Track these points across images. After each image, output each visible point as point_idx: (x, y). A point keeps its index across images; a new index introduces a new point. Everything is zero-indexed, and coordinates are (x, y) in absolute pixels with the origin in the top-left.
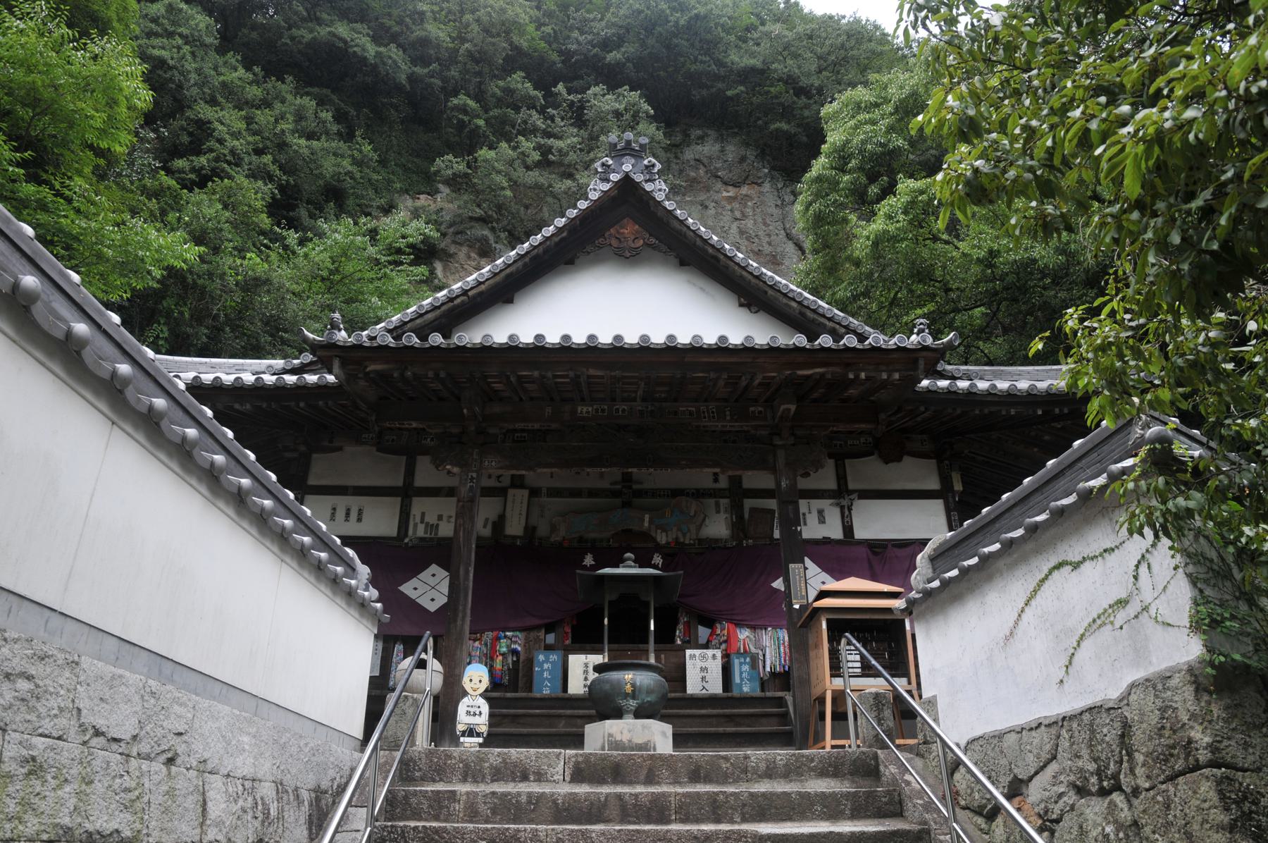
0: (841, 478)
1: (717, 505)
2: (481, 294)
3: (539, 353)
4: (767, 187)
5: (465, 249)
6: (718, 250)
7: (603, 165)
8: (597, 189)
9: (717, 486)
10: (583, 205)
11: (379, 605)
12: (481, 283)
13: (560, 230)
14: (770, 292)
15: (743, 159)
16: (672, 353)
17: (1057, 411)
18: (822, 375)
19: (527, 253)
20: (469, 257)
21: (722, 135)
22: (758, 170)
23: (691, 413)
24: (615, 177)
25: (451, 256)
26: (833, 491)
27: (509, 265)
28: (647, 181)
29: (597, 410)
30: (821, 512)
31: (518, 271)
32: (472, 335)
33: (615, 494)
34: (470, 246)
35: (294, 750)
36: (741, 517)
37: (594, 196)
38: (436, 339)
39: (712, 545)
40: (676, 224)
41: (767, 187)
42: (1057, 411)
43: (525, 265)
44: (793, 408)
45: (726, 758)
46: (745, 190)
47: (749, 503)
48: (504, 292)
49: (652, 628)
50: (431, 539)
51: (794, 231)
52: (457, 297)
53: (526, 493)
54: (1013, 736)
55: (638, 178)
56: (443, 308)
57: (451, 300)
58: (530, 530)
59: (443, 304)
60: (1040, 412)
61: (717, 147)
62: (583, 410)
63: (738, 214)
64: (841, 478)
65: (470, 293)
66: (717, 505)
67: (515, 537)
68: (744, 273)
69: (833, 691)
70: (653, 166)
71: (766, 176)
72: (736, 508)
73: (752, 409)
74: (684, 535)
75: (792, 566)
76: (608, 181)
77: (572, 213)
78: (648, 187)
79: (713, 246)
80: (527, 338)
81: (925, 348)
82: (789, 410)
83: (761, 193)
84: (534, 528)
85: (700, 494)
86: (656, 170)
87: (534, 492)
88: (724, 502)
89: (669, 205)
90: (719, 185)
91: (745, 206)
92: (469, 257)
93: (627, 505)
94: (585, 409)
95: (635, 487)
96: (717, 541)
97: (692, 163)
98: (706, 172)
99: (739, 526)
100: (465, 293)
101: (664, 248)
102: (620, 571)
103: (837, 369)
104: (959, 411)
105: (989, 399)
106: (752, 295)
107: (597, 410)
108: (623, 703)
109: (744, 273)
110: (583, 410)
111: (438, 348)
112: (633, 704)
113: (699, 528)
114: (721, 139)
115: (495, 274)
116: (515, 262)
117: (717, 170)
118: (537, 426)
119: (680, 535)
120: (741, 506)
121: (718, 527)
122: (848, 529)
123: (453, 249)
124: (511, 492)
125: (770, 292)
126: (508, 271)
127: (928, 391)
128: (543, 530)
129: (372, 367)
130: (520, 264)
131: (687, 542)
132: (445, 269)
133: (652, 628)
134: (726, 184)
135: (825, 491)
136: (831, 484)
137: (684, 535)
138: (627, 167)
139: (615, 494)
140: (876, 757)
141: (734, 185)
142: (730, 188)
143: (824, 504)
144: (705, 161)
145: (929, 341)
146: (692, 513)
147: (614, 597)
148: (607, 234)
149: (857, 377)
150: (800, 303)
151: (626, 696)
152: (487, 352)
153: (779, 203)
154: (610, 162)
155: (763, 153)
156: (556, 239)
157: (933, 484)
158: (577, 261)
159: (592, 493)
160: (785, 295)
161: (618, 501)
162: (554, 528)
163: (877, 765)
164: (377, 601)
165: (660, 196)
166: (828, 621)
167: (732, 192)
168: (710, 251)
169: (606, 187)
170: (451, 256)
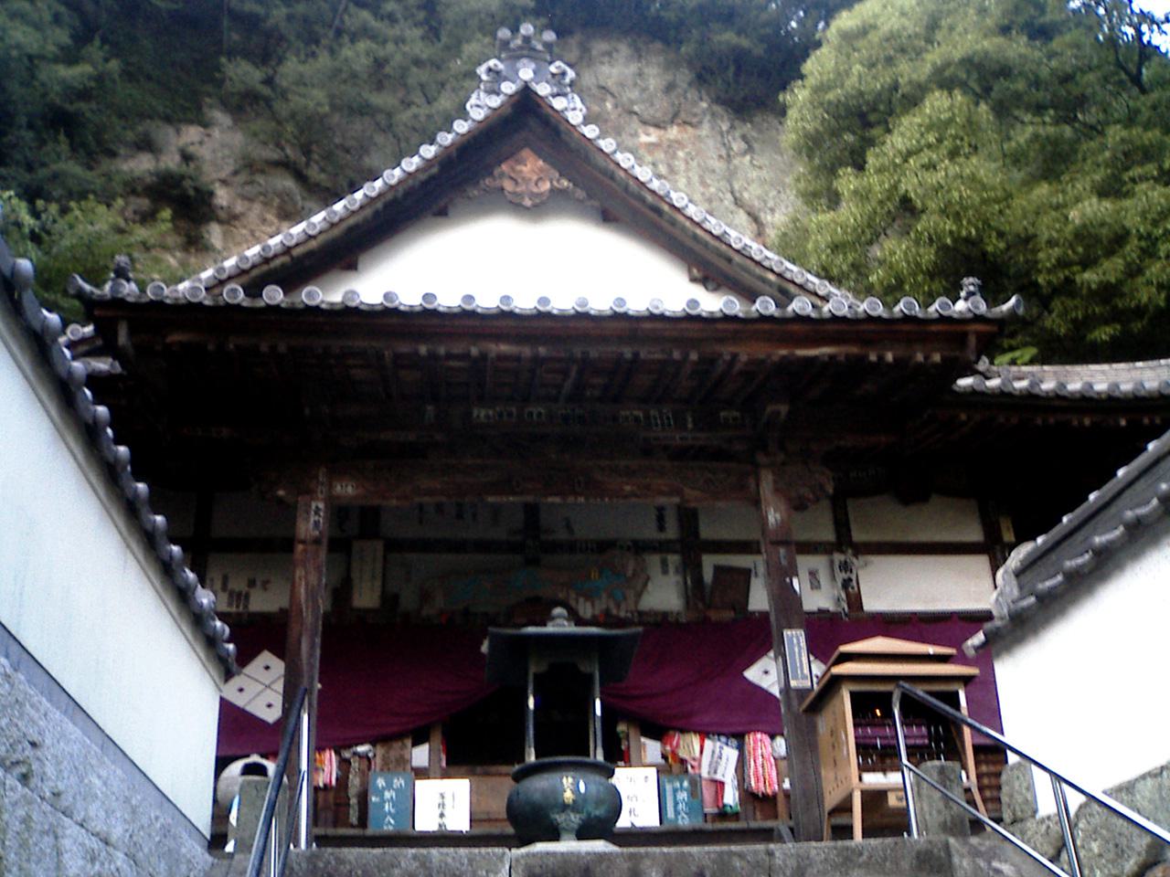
0: (842, 526)
1: (664, 564)
2: (310, 254)
3: (425, 323)
4: (705, 130)
5: (257, 208)
6: (661, 198)
7: (490, 70)
8: (481, 106)
9: (663, 536)
10: (461, 127)
11: (231, 647)
12: (311, 237)
13: (428, 163)
14: (737, 258)
15: (670, 88)
16: (623, 326)
17: (1146, 421)
18: (832, 357)
19: (380, 195)
20: (264, 221)
21: (637, 50)
22: (695, 104)
23: (637, 419)
24: (508, 88)
25: (236, 217)
26: (829, 543)
27: (353, 212)
28: (554, 96)
29: (501, 415)
30: (813, 574)
31: (366, 221)
32: (330, 293)
33: (514, 548)
34: (265, 204)
35: (145, 821)
36: (698, 580)
37: (478, 115)
38: (274, 295)
39: (661, 623)
40: (600, 160)
41: (705, 130)
42: (1146, 421)
43: (377, 213)
44: (783, 409)
45: (741, 856)
46: (674, 132)
47: (709, 562)
48: (347, 250)
49: (598, 712)
50: (239, 614)
51: (746, 195)
52: (276, 256)
53: (379, 546)
54: (1150, 782)
55: (543, 89)
56: (255, 273)
57: (266, 260)
58: (389, 600)
59: (254, 266)
60: (1123, 423)
61: (633, 68)
62: (480, 413)
63: (663, 169)
64: (842, 526)
65: (296, 252)
66: (664, 564)
67: (367, 611)
68: (699, 232)
69: (863, 793)
70: (564, 74)
71: (704, 113)
72: (691, 566)
73: (722, 414)
74: (618, 606)
75: (787, 633)
76: (498, 93)
77: (446, 139)
78: (559, 104)
79: (653, 192)
80: (410, 298)
81: (978, 319)
82: (778, 413)
83: (699, 138)
84: (396, 597)
85: (641, 548)
86: (567, 80)
87: (393, 546)
88: (674, 559)
89: (591, 131)
90: (635, 124)
91: (674, 156)
92: (264, 221)
93: (533, 562)
94: (483, 413)
95: (543, 537)
96: (665, 615)
97: (595, 91)
98: (616, 106)
99: (695, 591)
100: (287, 250)
101: (580, 194)
102: (550, 629)
103: (854, 350)
104: (1014, 420)
105: (1057, 403)
106: (708, 262)
107: (501, 415)
108: (560, 818)
109: (699, 232)
110: (480, 413)
111: (276, 309)
112: (575, 819)
113: (639, 595)
114: (638, 54)
115: (333, 225)
116: (362, 207)
117: (632, 102)
118: (412, 437)
119: (612, 606)
120: (699, 565)
121: (664, 594)
122: (855, 601)
123: (239, 207)
124: (356, 546)
125: (737, 258)
126: (352, 221)
127: (973, 392)
128: (408, 601)
129: (175, 338)
130: (368, 212)
131: (622, 614)
132: (225, 235)
133: (598, 712)
134: (645, 123)
135: (820, 544)
136: (828, 535)
137: (618, 606)
138: (526, 73)
139: (514, 548)
140: (947, 846)
141: (657, 126)
142: (651, 130)
143: (818, 562)
144: (614, 89)
145: (983, 308)
146: (630, 573)
147: (543, 668)
148: (497, 172)
149: (881, 358)
150: (780, 275)
151: (564, 807)
152: (351, 316)
153: (724, 152)
154: (501, 66)
155: (702, 78)
156: (423, 177)
157: (975, 534)
158: (451, 211)
159: (483, 546)
160: (758, 263)
161: (519, 558)
162: (425, 597)
163: (949, 855)
164: (229, 641)
165: (575, 118)
166: (853, 694)
167: (652, 136)
168: (649, 198)
169: (495, 102)
170: (236, 217)
